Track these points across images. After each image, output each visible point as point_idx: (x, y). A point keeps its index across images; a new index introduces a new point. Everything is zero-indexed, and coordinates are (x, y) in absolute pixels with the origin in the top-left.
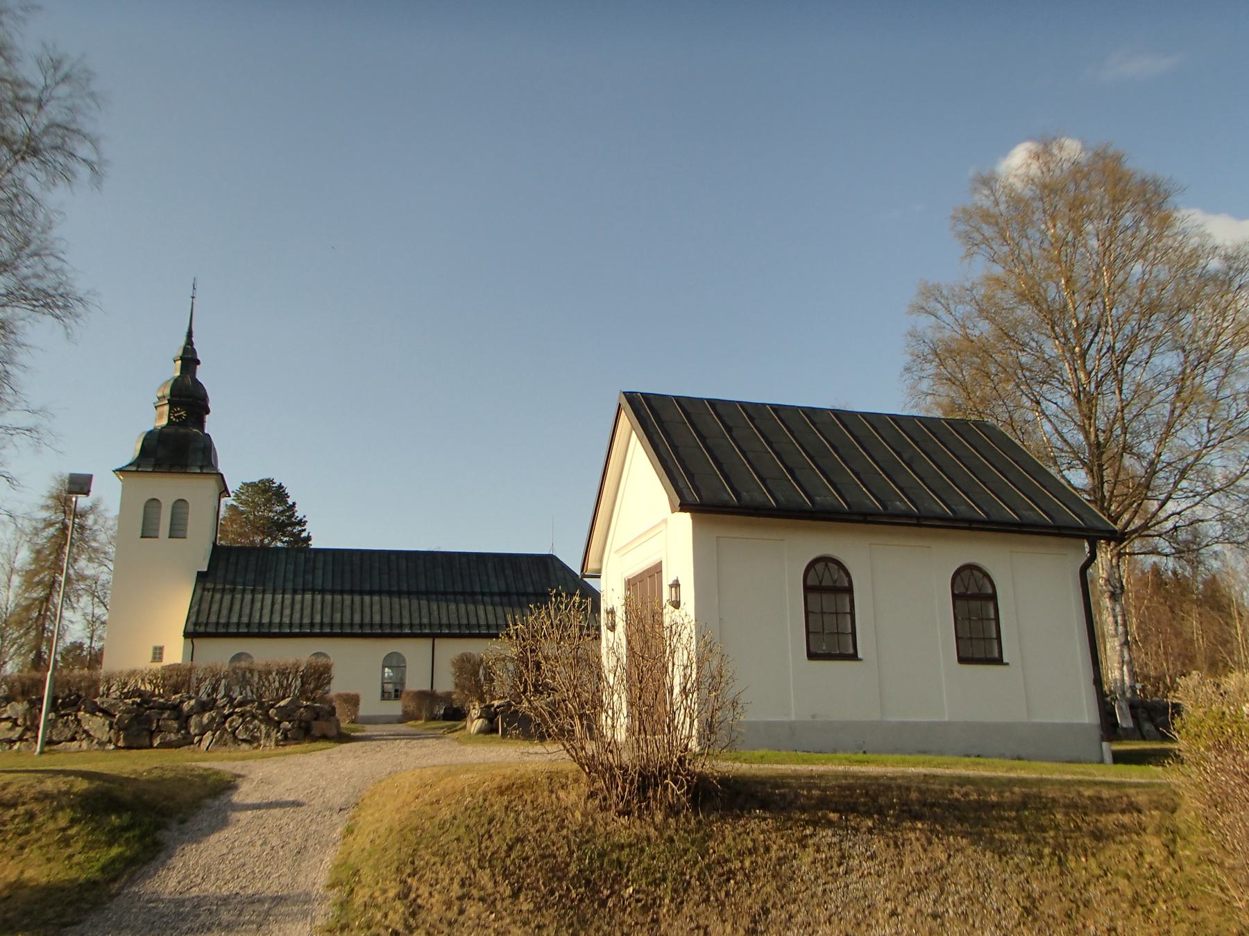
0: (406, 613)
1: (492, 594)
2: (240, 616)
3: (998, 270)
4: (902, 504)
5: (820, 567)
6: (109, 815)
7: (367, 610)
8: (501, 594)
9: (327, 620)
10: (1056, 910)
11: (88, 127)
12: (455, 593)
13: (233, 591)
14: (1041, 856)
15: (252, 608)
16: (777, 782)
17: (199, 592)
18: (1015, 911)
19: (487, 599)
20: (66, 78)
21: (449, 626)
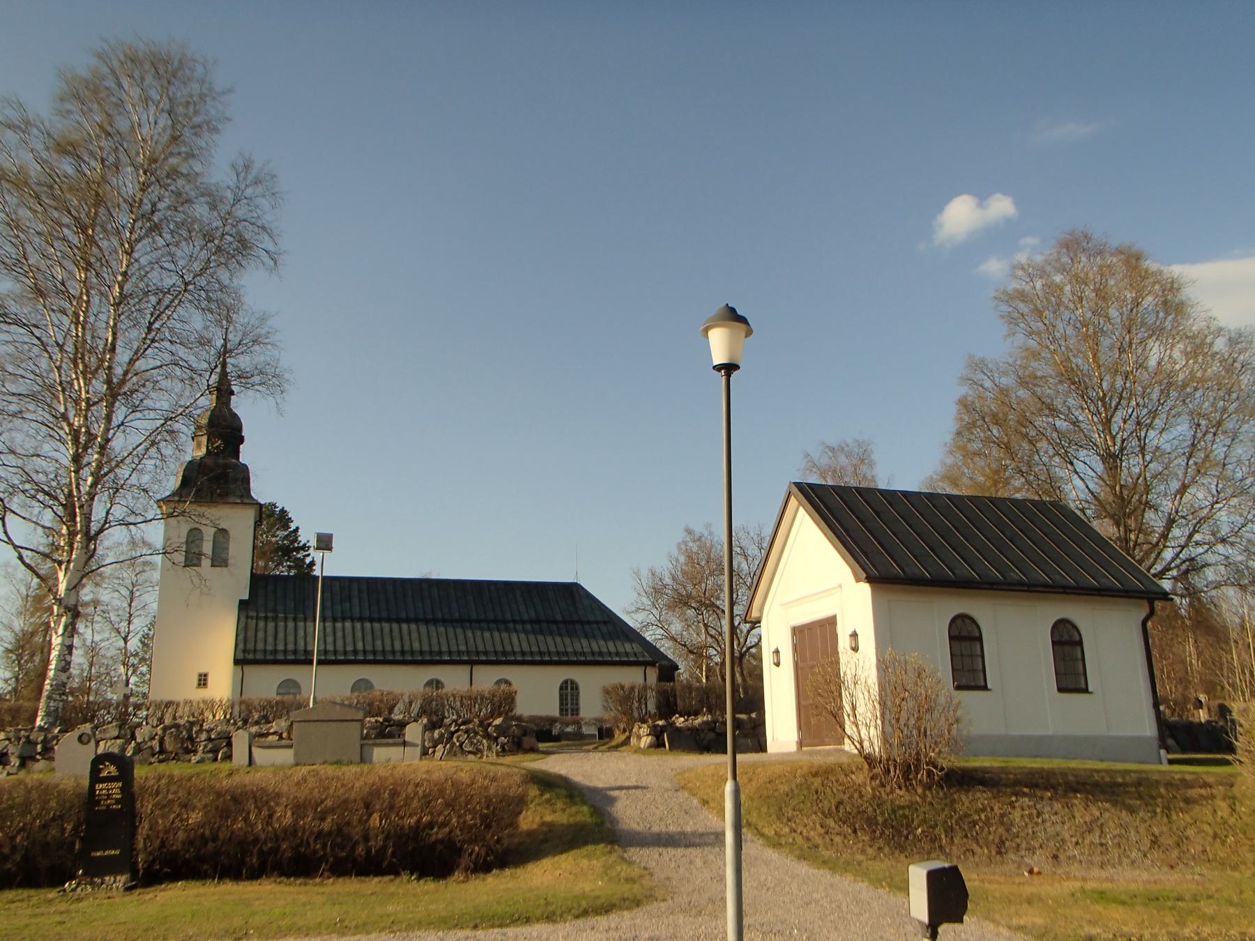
0: (443, 641)
1: (523, 622)
2: (286, 644)
3: (1032, 343)
4: (1016, 575)
5: (959, 621)
6: (1208, 722)
7: (406, 638)
8: (532, 622)
9: (369, 648)
10: (1170, 842)
11: (267, 219)
12: (488, 621)
13: (275, 619)
14: (1155, 813)
15: (296, 636)
16: (984, 770)
17: (243, 620)
18: (1146, 842)
19: (519, 627)
20: (257, 182)
21: (486, 653)
